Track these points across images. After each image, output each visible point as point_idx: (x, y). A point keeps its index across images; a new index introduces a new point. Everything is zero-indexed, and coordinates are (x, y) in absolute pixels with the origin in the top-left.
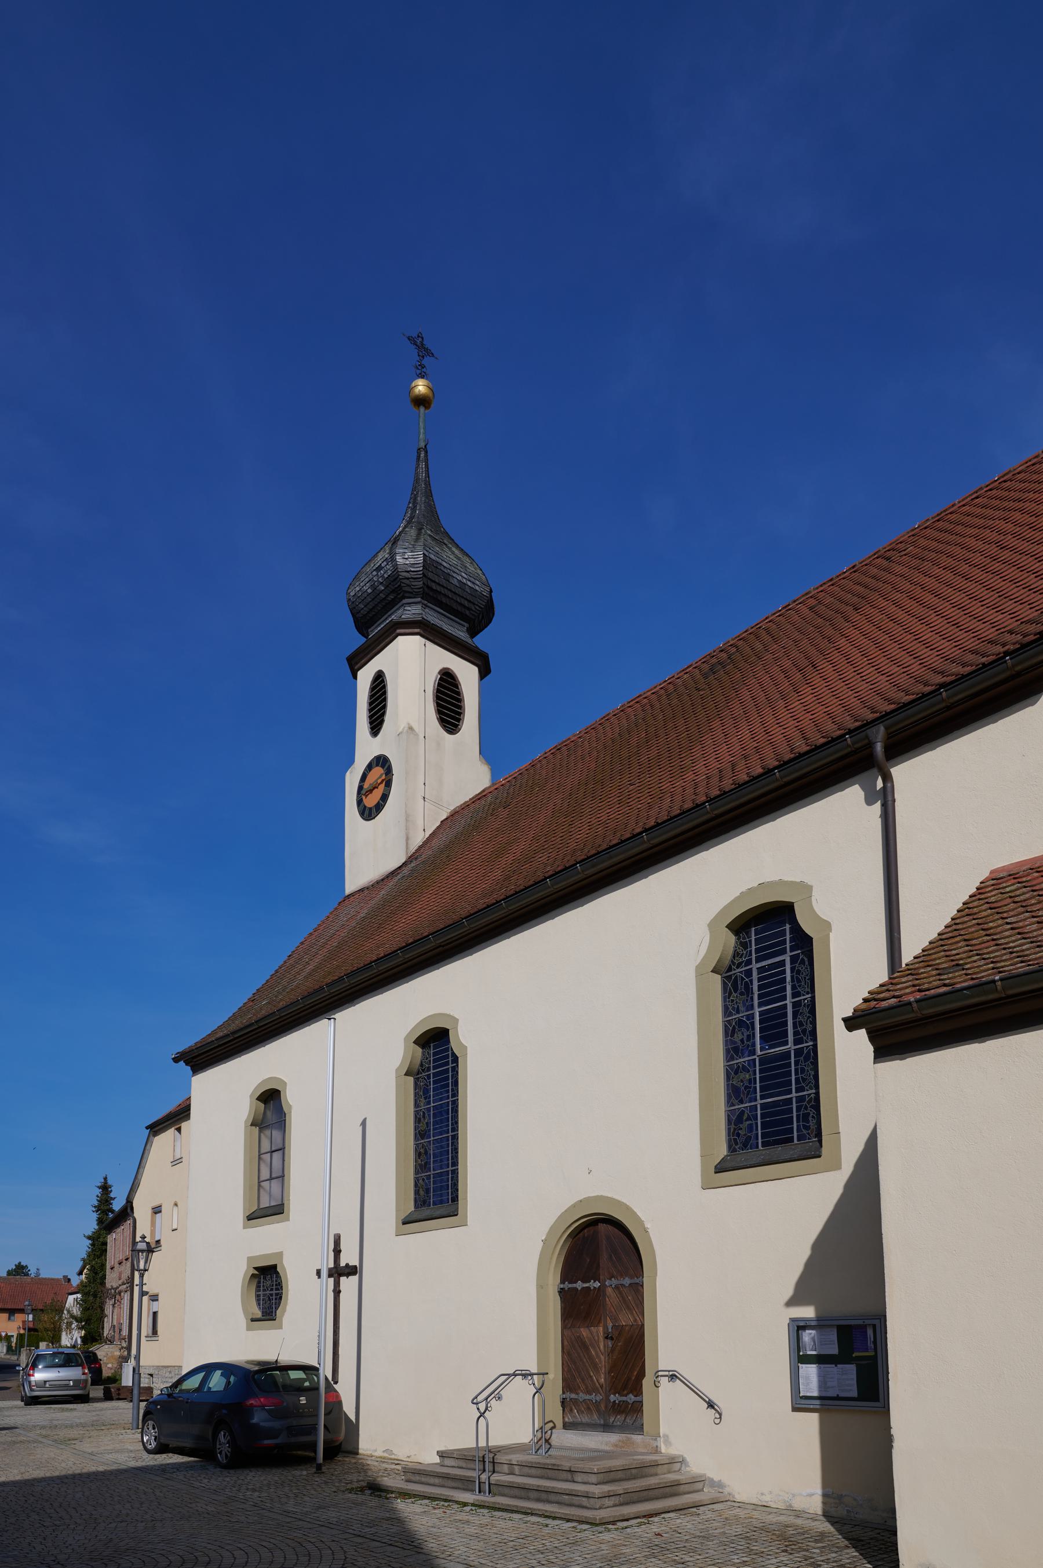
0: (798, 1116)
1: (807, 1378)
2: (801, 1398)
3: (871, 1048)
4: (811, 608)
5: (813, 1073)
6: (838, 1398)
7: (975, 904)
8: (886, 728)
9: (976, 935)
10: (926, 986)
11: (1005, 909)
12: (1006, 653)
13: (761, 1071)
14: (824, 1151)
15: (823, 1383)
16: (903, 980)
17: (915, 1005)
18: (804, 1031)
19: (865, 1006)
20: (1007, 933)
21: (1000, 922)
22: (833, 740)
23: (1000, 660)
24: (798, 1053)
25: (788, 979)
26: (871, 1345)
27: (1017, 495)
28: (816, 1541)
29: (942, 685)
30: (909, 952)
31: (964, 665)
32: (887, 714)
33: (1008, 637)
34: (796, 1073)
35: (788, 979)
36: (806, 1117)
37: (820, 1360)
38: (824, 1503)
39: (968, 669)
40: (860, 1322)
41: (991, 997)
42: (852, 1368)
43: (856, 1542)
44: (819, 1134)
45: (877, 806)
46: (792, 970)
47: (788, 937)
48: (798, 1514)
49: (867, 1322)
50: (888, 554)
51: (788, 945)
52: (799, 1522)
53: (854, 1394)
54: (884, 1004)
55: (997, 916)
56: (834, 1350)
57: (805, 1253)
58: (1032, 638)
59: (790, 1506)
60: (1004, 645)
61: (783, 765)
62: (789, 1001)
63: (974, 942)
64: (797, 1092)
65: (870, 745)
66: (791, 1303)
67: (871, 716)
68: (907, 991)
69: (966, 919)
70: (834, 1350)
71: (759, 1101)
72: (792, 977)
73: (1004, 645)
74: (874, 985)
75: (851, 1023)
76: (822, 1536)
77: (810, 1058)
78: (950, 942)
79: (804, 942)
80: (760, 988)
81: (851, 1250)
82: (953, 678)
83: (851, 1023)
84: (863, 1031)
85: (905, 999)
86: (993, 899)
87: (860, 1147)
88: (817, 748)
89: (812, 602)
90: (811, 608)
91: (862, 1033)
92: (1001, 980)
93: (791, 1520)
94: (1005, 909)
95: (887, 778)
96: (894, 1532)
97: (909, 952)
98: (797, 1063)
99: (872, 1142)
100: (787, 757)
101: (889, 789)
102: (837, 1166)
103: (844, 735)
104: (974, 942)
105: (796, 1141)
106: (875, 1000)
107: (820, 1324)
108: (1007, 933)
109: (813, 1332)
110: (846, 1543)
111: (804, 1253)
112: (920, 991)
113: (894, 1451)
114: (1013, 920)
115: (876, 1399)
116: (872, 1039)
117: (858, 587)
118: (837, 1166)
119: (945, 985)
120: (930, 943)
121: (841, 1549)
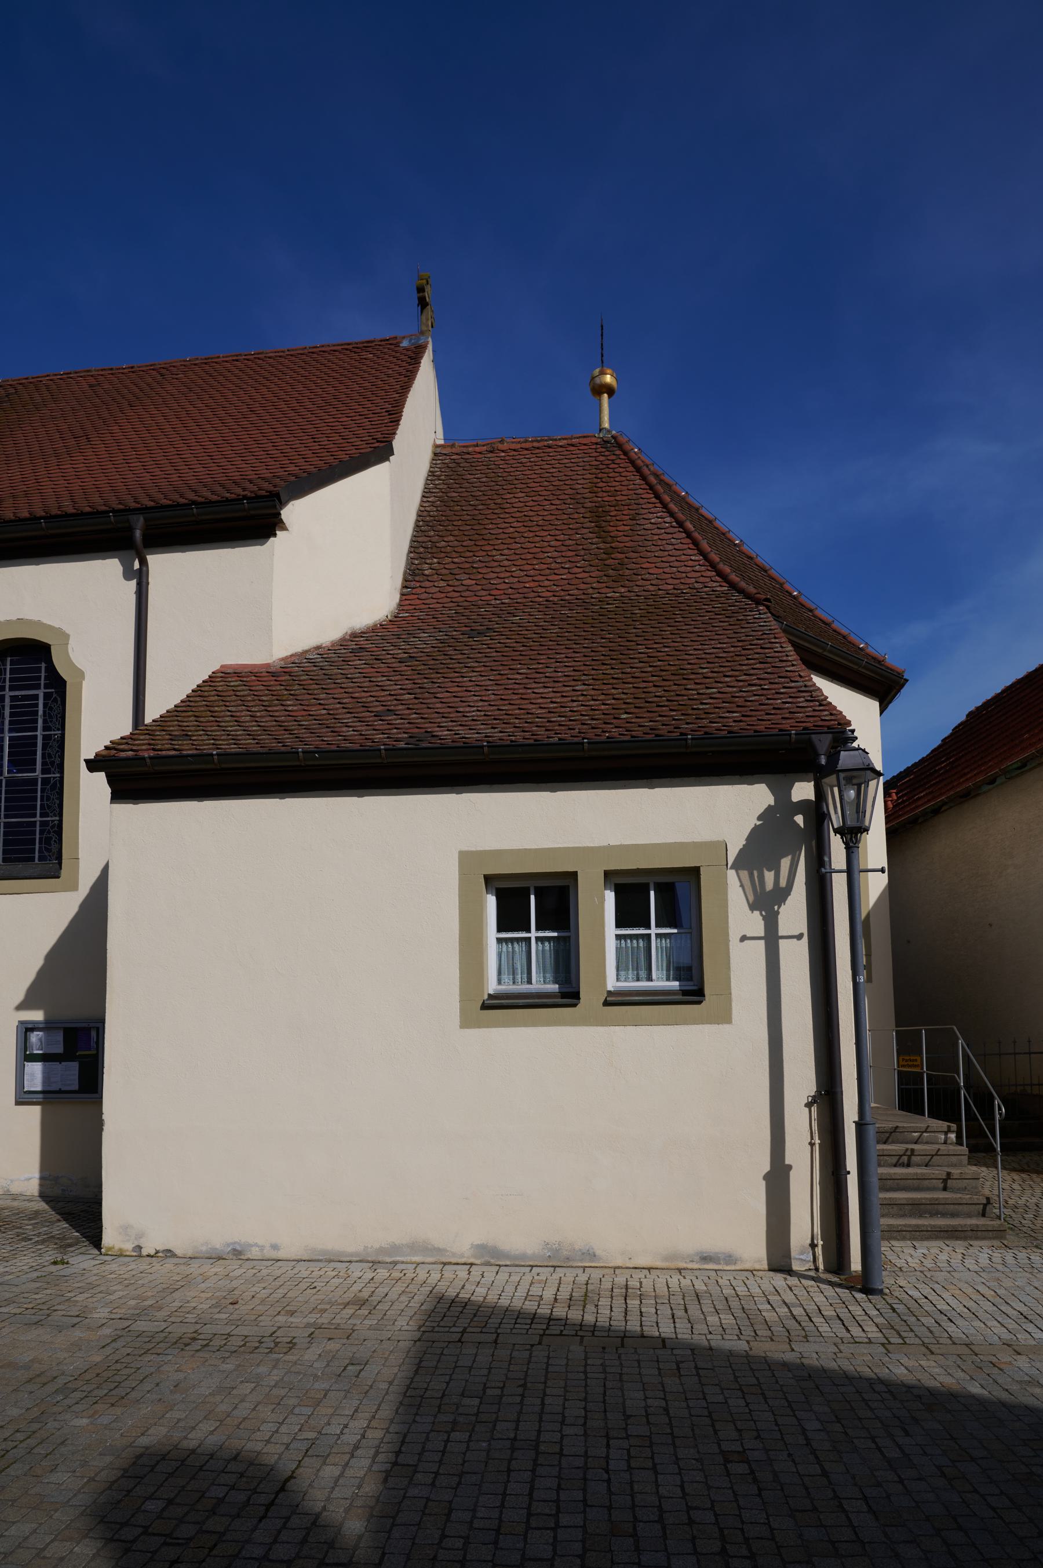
0: (41, 839)
1: (32, 1075)
2: (26, 1092)
3: (108, 790)
4: (91, 386)
5: (58, 802)
6: (60, 1092)
7: (207, 688)
8: (145, 520)
9: (204, 714)
10: (159, 747)
11: (228, 699)
12: (245, 497)
13: (36, 791)
14: (63, 872)
15: (46, 1078)
16: (142, 737)
17: (148, 761)
18: (52, 763)
19: (105, 753)
20: (227, 719)
21: (223, 708)
22: (98, 512)
23: (239, 500)
24: (45, 781)
25: (41, 713)
26: (93, 1044)
27: (266, 374)
28: (30, 1219)
29: (194, 503)
30: (152, 714)
31: (228, 491)
32: (147, 508)
33: (247, 485)
34: (42, 800)
35: (41, 713)
36: (48, 841)
37: (44, 1058)
38: (41, 1185)
39: (215, 498)
40: (86, 1025)
41: (209, 766)
42: (74, 1066)
43: (67, 1216)
44: (59, 858)
45: (133, 583)
46: (45, 705)
47: (43, 675)
48: (15, 1197)
49: (91, 1025)
50: (163, 371)
51: (42, 682)
52: (15, 1204)
53: (76, 1087)
54: (123, 755)
55: (221, 703)
56: (59, 1049)
57: (39, 962)
58: (263, 493)
59: (8, 1190)
60: (244, 489)
61: (49, 518)
62: (39, 733)
63: (202, 719)
64: (41, 816)
65: (131, 530)
66: (20, 1007)
67: (133, 505)
68: (144, 747)
69: (198, 699)
70: (59, 1049)
71: (38, 818)
72: (44, 712)
73: (244, 489)
74: (116, 737)
75: (93, 765)
76: (37, 1213)
77: (57, 788)
78: (184, 714)
79: (58, 685)
80: (12, 715)
81: (80, 960)
82: (203, 500)
83: (93, 765)
84: (103, 774)
85: (141, 754)
86: (220, 688)
87: (96, 874)
88: (82, 514)
89: (92, 381)
90: (91, 386)
91: (102, 775)
92: (218, 754)
93: (9, 1203)
94: (228, 699)
95: (143, 562)
96: (99, 1202)
97: (152, 714)
98: (43, 791)
99: (105, 871)
100: (55, 511)
101: (144, 573)
102: (74, 887)
103: (108, 512)
104: (202, 719)
105: (36, 861)
106: (116, 749)
107: (47, 1026)
108: (227, 719)
109: (41, 1033)
110: (59, 1217)
111: (37, 962)
112: (154, 749)
113: (104, 1134)
114: (233, 709)
115: (96, 1092)
116: (109, 782)
117: (134, 387)
118: (74, 887)
119: (174, 749)
120: (168, 711)
121: (52, 1223)
